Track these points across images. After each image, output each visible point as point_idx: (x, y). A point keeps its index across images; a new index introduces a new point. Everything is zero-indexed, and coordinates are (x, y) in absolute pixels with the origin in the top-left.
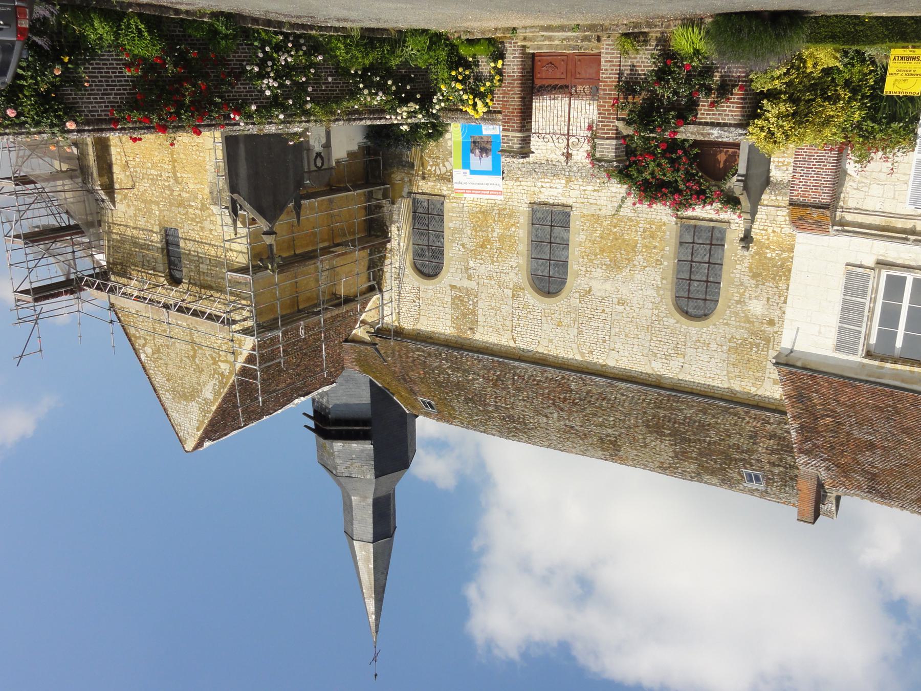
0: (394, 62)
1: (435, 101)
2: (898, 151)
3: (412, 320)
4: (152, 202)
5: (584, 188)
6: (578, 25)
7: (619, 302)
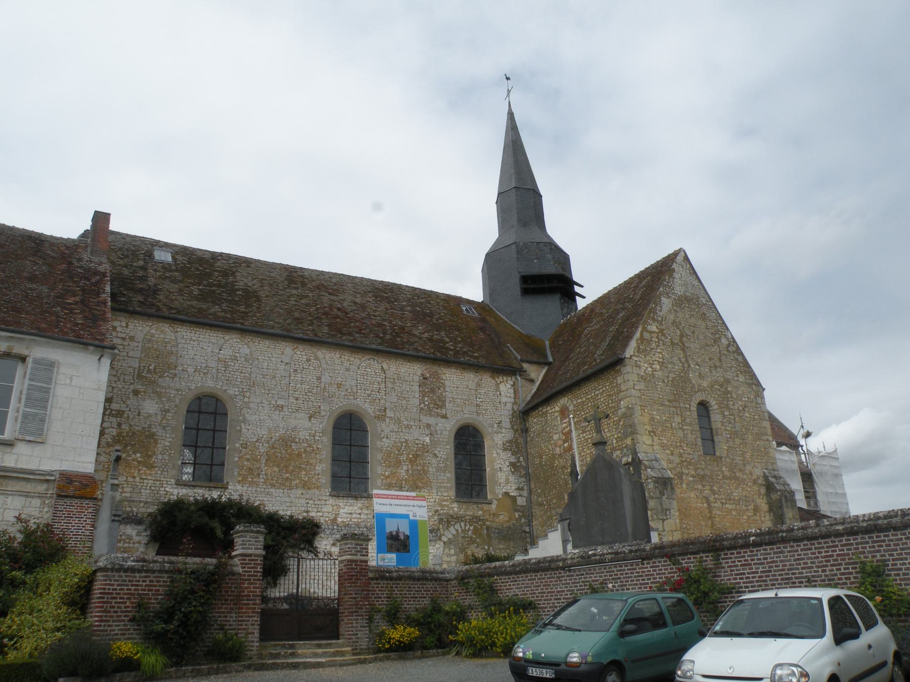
4: (730, 478)
5: (318, 514)
7: (282, 408)
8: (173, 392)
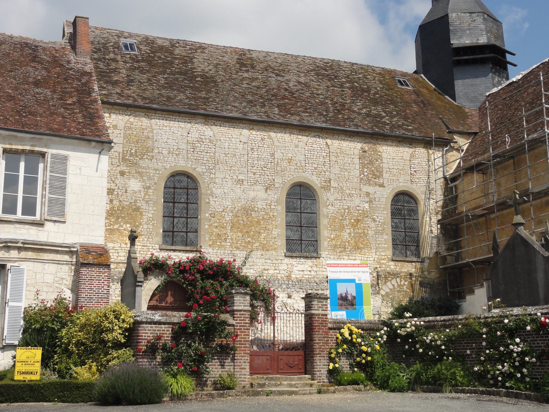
0: (418, 366)
1: (385, 337)
2: (35, 308)
3: (417, 156)
5: (276, 271)
6: (267, 395)
7: (243, 182)
8: (151, 171)
